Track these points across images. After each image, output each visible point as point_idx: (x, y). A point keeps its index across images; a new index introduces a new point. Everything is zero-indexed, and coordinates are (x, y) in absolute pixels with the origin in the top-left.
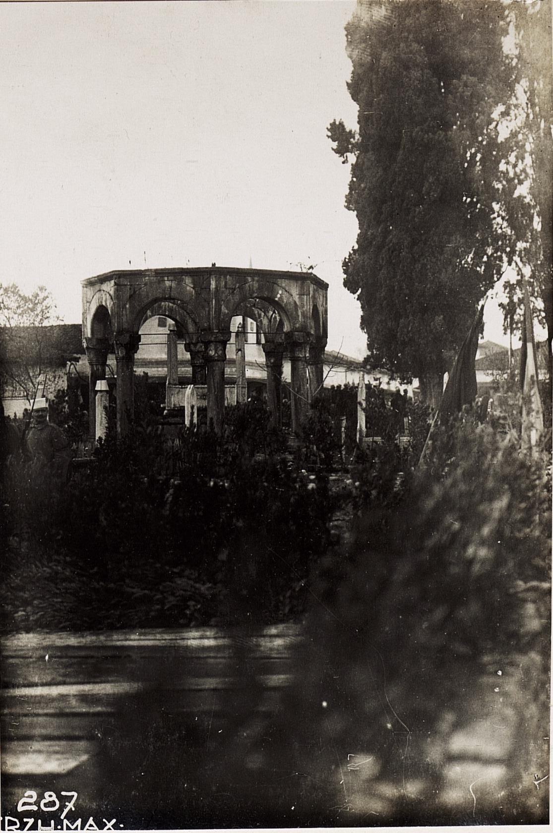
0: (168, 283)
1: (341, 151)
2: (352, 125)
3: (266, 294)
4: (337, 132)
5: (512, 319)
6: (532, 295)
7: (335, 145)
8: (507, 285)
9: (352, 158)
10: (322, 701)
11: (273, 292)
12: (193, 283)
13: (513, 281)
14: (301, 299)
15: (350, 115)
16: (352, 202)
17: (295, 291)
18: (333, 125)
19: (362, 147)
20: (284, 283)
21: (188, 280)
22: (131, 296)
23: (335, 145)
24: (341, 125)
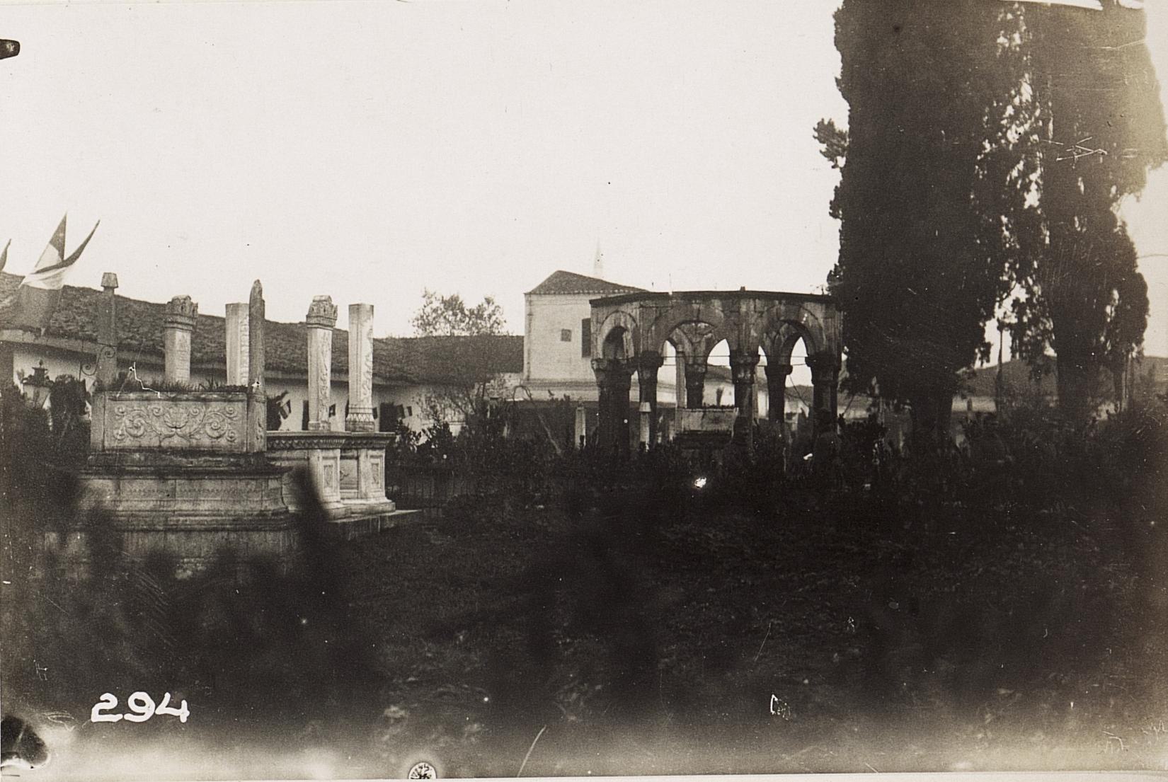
0: (695, 306)
1: (830, 155)
2: (842, 125)
3: (793, 318)
4: (825, 132)
5: (1021, 341)
6: (1043, 316)
7: (824, 147)
8: (1016, 303)
9: (842, 161)
10: (697, 490)
11: (799, 316)
12: (723, 306)
13: (1023, 300)
14: (826, 323)
15: (840, 114)
16: (835, 208)
17: (820, 314)
18: (821, 124)
19: (850, 153)
20: (809, 306)
21: (717, 303)
22: (657, 318)
23: (824, 147)
24: (831, 124)
